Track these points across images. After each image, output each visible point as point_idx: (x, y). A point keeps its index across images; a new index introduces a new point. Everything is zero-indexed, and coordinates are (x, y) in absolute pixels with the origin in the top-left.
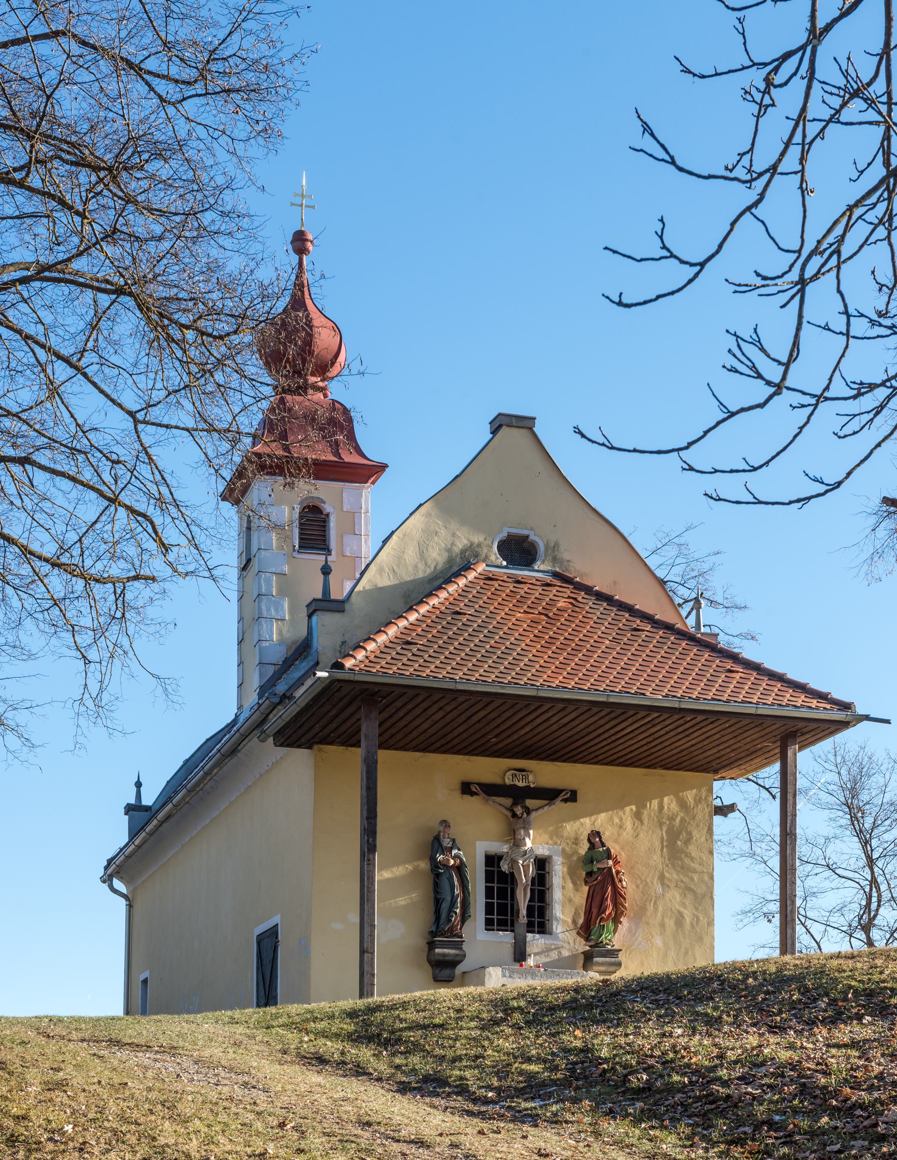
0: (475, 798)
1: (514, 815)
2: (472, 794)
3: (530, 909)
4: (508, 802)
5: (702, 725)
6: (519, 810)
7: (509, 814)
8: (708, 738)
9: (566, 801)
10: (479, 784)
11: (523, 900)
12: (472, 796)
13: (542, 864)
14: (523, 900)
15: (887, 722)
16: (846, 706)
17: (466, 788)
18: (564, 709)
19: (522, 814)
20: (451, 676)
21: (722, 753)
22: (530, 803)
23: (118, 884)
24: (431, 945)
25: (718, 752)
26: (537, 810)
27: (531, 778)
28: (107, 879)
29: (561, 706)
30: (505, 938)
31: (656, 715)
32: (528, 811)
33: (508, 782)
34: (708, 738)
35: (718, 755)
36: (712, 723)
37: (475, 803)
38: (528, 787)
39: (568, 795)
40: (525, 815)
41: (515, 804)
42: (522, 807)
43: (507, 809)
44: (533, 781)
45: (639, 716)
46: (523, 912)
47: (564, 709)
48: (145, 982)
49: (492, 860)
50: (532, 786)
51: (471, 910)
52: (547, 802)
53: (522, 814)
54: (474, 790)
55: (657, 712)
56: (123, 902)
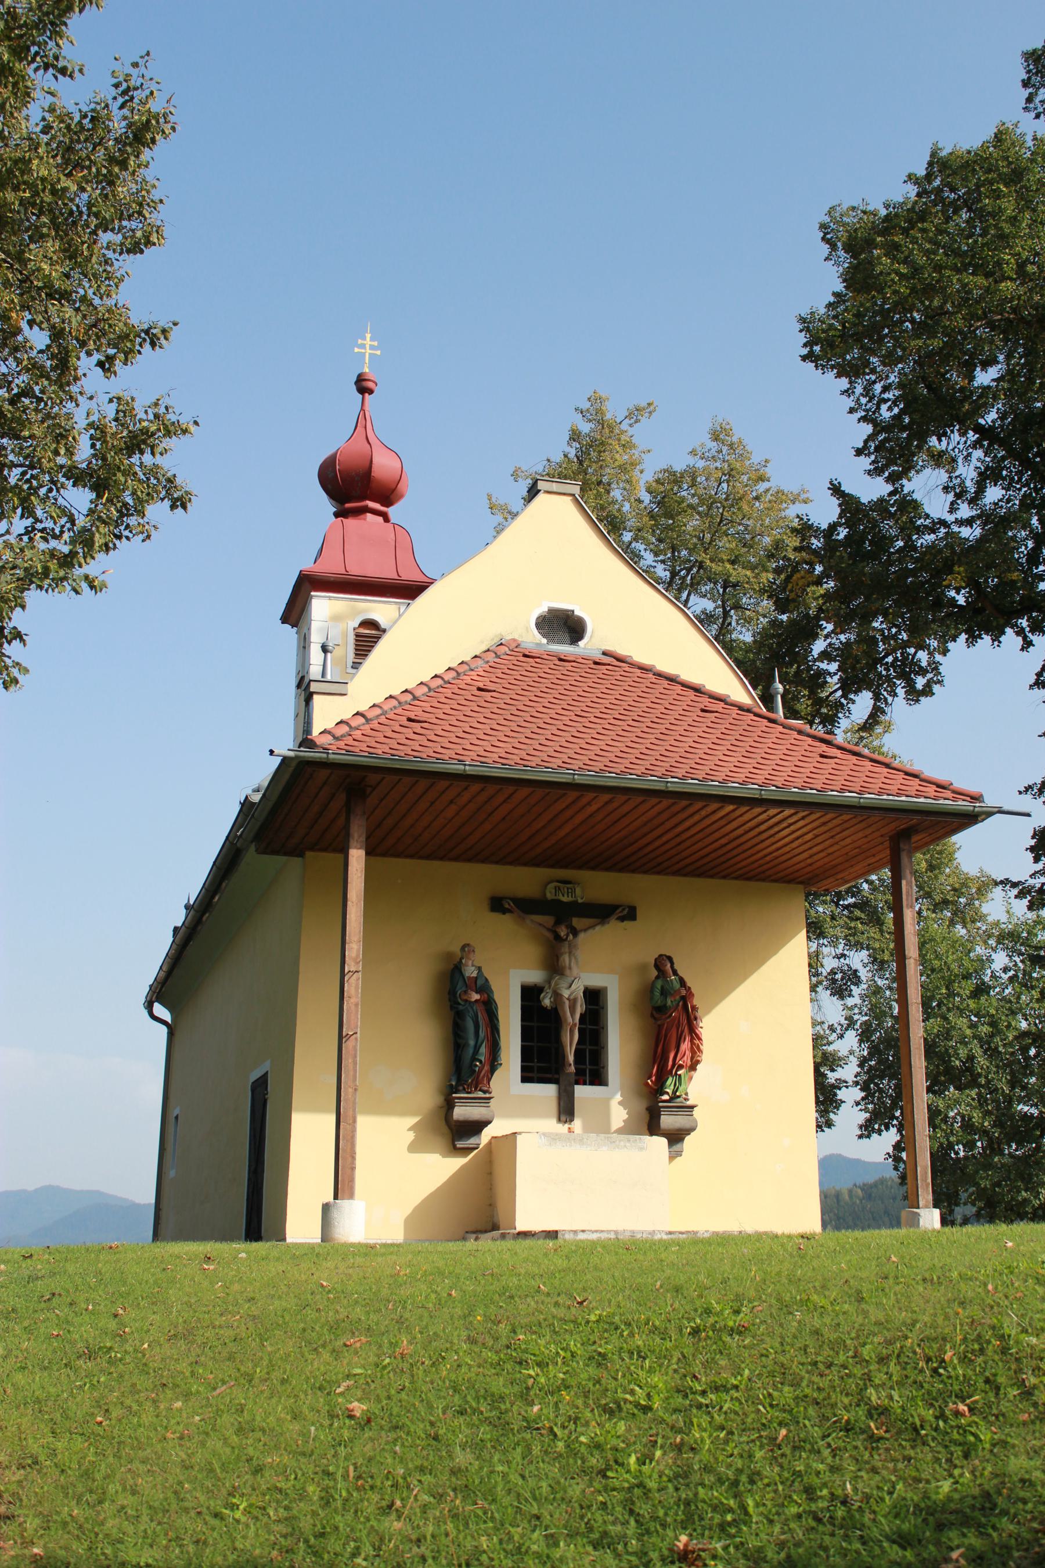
0: (507, 916)
1: (558, 938)
2: (504, 911)
3: (578, 1054)
4: (548, 920)
5: (791, 821)
6: (563, 932)
7: (550, 935)
8: (797, 838)
9: (622, 919)
10: (512, 899)
11: (571, 1042)
12: (504, 913)
13: (595, 997)
14: (571, 1042)
15: (1028, 815)
16: (976, 798)
17: (497, 905)
18: (610, 801)
19: (567, 935)
20: (461, 758)
21: (816, 858)
22: (576, 922)
23: (159, 1010)
24: (449, 1105)
25: (811, 857)
26: (585, 930)
27: (578, 891)
28: (149, 1006)
29: (606, 797)
30: (550, 1090)
31: (731, 807)
32: (575, 932)
33: (549, 896)
34: (797, 838)
35: (809, 861)
36: (803, 818)
37: (505, 923)
38: (575, 903)
39: (625, 912)
40: (571, 937)
41: (558, 922)
42: (567, 927)
43: (549, 930)
44: (581, 895)
45: (709, 809)
46: (571, 1058)
47: (610, 801)
48: (177, 1118)
49: (530, 994)
50: (580, 901)
51: (502, 1056)
52: (599, 920)
53: (567, 935)
54: (507, 906)
55: (732, 803)
56: (164, 1030)
